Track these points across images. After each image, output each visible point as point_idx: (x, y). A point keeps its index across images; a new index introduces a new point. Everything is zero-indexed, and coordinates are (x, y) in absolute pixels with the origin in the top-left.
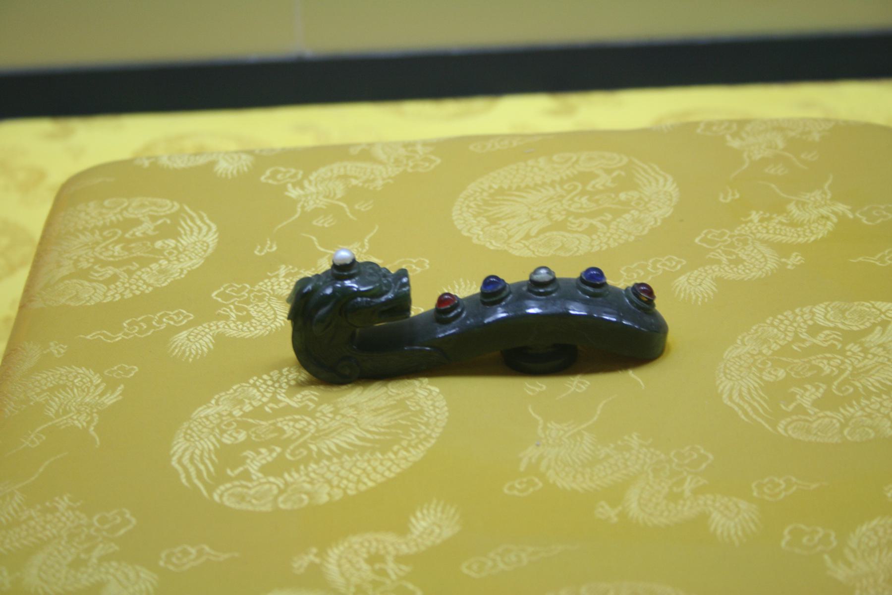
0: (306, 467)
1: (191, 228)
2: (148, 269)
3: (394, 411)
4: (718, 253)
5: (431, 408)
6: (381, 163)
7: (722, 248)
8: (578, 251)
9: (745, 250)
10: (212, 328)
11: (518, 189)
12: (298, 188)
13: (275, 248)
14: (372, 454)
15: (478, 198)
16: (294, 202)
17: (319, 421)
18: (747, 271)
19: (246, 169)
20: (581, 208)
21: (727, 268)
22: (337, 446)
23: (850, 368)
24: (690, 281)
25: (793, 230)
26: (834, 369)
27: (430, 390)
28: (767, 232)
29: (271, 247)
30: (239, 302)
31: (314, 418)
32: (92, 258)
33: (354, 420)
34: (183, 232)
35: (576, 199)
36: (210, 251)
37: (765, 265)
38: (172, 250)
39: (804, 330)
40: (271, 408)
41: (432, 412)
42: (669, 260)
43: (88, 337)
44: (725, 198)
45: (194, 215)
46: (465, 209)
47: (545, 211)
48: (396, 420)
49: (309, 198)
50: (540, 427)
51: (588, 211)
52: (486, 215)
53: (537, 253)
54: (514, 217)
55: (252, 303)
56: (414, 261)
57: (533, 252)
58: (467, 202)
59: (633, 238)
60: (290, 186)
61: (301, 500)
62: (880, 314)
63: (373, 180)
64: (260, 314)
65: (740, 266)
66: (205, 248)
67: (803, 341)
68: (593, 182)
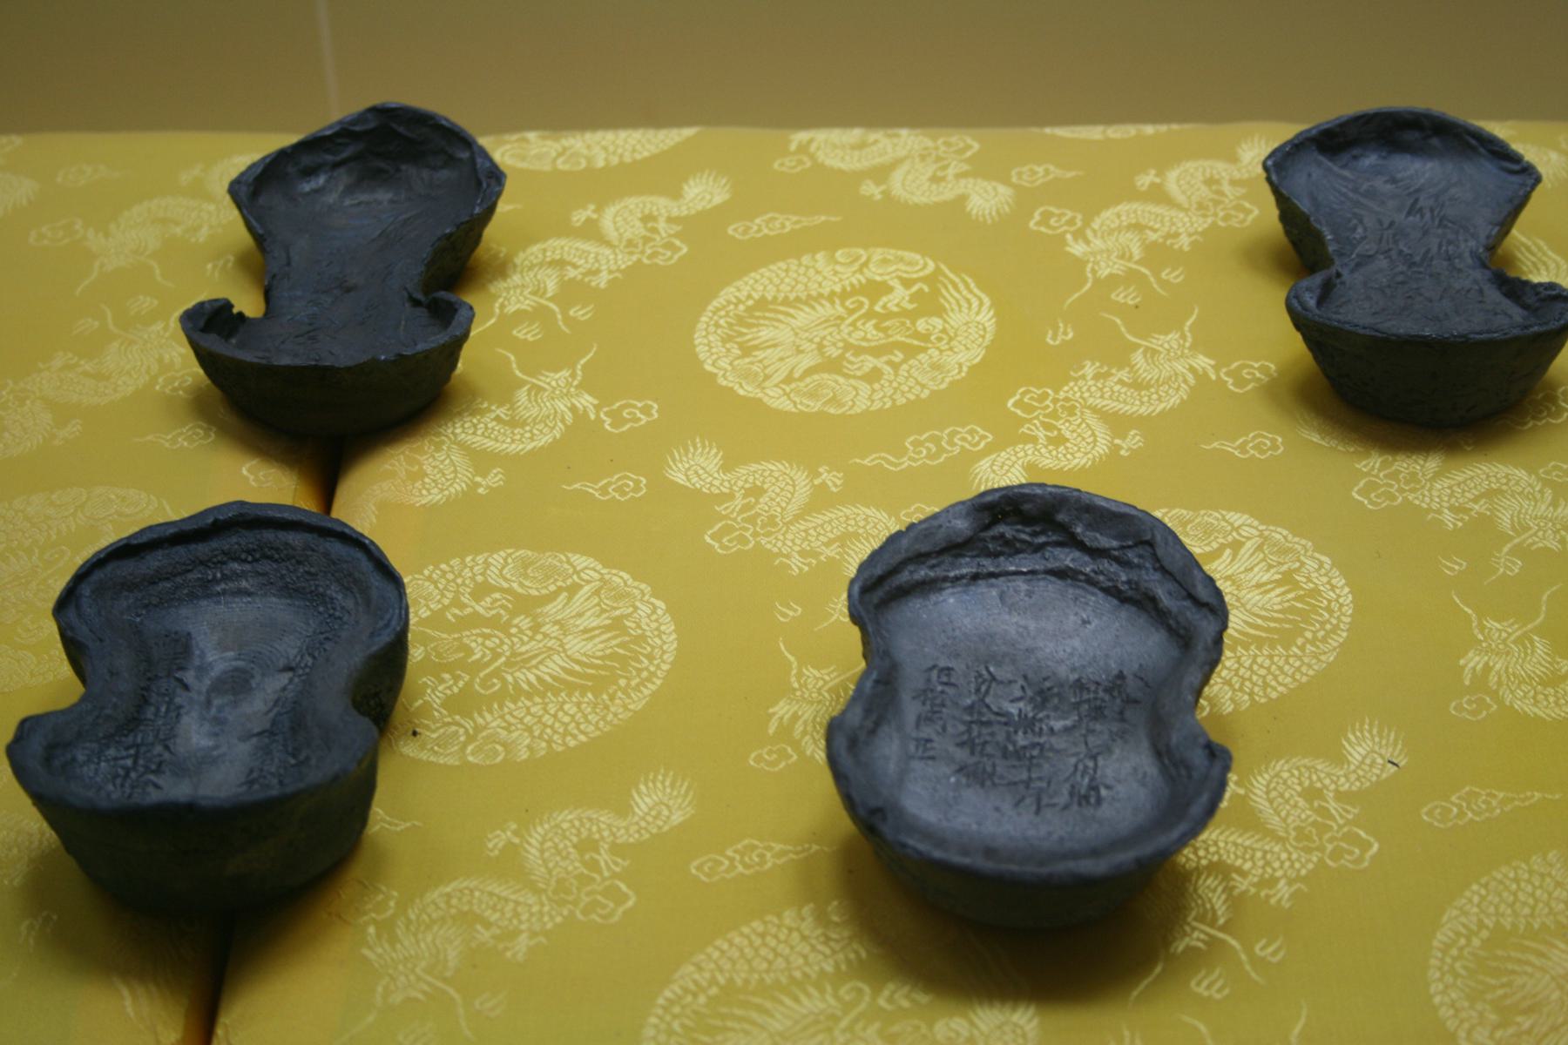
0: (501, 707)
1: (968, 301)
2: (917, 362)
3: (609, 635)
4: (1035, 425)
5: (713, 345)
6: (609, 244)
7: (1041, 417)
8: (853, 406)
9: (435, 459)
10: (1019, 455)
11: (786, 302)
12: (1080, 241)
13: (1070, 335)
14: (1273, 648)
15: (731, 314)
16: (1079, 263)
17: (515, 640)
18: (1069, 456)
19: (1007, 209)
20: (864, 339)
21: (1043, 450)
22: (538, 678)
23: (842, 327)
24: (994, 468)
25: (1136, 394)
26: (488, 652)
27: (652, 604)
28: (1102, 397)
29: (1065, 333)
30: (1045, 416)
31: (510, 636)
32: (840, 341)
33: (559, 643)
34: (947, 306)
35: (859, 324)
36: (989, 337)
37: (1093, 448)
38: (940, 335)
39: (468, 590)
40: (455, 615)
41: (1331, 593)
42: (971, 432)
43: (866, 462)
44: (1054, 338)
45: (957, 280)
46: (712, 329)
47: (817, 340)
48: (1288, 601)
49: (512, 292)
50: (794, 672)
51: (873, 344)
52: (738, 340)
53: (799, 406)
54: (775, 346)
55: (1061, 418)
56: (639, 405)
57: (795, 403)
58: (715, 318)
59: (926, 392)
60: (1069, 237)
61: (496, 753)
62: (1232, 531)
63: (1177, 235)
64: (1075, 435)
65: (1061, 448)
66: (982, 333)
67: (464, 606)
68: (885, 299)
